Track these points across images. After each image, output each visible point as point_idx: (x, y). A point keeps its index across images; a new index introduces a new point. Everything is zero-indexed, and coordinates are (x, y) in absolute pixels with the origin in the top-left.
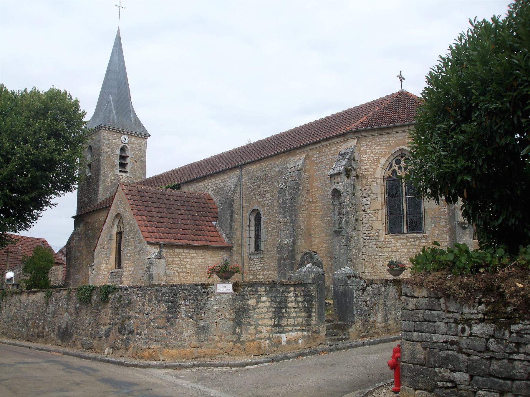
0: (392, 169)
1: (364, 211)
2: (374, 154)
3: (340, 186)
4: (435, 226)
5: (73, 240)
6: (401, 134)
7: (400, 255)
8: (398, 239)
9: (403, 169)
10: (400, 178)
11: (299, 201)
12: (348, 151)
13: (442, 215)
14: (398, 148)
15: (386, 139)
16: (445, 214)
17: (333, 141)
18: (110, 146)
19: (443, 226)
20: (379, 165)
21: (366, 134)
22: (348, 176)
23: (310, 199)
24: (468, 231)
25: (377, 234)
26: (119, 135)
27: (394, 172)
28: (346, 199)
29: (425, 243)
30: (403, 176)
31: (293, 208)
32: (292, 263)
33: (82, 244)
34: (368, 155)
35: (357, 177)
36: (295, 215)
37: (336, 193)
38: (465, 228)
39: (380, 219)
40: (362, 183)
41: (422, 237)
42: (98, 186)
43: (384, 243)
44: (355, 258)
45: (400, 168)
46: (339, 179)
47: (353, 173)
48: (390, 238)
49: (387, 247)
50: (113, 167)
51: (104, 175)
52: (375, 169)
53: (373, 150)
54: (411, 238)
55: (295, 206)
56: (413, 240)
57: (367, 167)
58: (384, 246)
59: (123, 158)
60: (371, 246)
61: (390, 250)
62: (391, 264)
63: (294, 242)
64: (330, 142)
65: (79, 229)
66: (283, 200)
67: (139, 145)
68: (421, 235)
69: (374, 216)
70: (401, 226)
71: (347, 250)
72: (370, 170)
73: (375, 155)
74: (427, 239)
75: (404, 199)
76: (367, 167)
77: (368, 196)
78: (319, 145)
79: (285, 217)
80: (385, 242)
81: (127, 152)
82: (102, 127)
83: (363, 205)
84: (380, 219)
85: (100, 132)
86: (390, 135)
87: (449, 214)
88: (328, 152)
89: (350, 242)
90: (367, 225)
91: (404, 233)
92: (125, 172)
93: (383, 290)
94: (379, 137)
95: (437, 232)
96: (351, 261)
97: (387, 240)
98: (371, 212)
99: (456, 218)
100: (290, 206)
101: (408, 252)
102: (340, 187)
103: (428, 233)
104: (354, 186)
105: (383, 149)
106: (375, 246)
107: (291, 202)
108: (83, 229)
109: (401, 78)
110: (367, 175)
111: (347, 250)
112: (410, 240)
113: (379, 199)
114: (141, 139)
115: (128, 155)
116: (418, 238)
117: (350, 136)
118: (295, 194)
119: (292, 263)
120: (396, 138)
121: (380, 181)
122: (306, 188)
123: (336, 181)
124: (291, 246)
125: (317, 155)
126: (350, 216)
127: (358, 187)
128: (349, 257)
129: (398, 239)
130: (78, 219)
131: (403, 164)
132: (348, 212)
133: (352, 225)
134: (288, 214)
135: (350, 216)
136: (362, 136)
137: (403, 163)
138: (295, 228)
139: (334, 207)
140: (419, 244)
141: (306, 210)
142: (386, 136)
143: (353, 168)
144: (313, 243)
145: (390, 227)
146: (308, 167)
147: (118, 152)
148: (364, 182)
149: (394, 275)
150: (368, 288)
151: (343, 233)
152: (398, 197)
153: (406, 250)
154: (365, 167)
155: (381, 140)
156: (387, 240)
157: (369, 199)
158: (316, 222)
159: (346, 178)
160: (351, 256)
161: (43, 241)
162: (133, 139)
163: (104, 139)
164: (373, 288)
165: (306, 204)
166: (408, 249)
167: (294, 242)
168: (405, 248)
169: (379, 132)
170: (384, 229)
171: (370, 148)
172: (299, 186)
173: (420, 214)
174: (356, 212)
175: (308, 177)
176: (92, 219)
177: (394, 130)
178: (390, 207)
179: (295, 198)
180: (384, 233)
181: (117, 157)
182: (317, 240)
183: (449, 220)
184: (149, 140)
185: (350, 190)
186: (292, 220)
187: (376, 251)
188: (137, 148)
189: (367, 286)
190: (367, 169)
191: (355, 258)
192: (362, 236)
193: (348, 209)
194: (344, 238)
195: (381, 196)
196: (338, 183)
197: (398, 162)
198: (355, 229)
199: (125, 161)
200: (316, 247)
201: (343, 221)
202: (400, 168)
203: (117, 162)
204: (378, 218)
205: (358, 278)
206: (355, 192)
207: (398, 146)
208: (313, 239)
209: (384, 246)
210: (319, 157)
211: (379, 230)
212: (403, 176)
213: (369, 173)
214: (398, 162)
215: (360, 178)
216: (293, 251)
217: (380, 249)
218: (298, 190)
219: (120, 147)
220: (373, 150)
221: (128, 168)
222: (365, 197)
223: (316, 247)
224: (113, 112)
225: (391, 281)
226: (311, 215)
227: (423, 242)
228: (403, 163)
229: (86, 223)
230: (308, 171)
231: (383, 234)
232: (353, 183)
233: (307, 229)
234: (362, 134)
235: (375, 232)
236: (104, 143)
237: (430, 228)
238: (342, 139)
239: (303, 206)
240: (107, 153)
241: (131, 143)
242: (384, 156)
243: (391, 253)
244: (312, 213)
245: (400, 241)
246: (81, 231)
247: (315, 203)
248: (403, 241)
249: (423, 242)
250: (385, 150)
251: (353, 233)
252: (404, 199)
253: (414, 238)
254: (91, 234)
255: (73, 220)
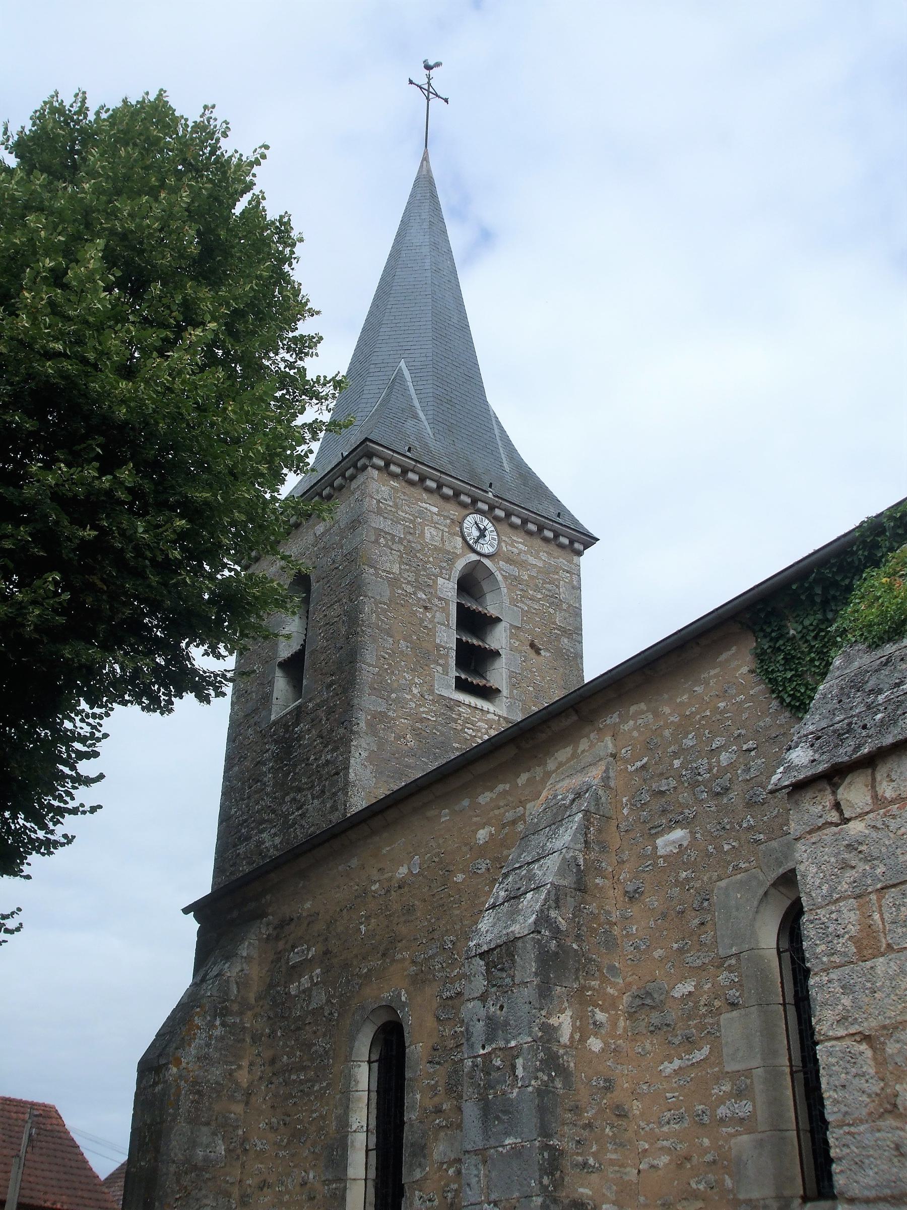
5: (184, 1043)
18: (410, 551)
26: (454, 511)
33: (243, 1077)
42: (343, 745)
50: (425, 656)
51: (381, 689)
59: (474, 622)
65: (232, 971)
67: (548, 571)
81: (489, 598)
82: (370, 455)
85: (361, 478)
92: (488, 693)
108: (256, 972)
114: (552, 547)
115: (492, 610)
130: (220, 918)
147: (448, 588)
161: (53, 1107)
162: (519, 544)
163: (379, 512)
176: (323, 897)
181: (445, 610)
184: (589, 559)
188: (537, 589)
199: (483, 641)
203: (448, 637)
219: (460, 564)
221: (498, 675)
224: (416, 417)
229: (283, 924)
236: (379, 532)
240: (394, 582)
241: (509, 561)
246: (243, 984)
254: (319, 998)
255: (192, 925)
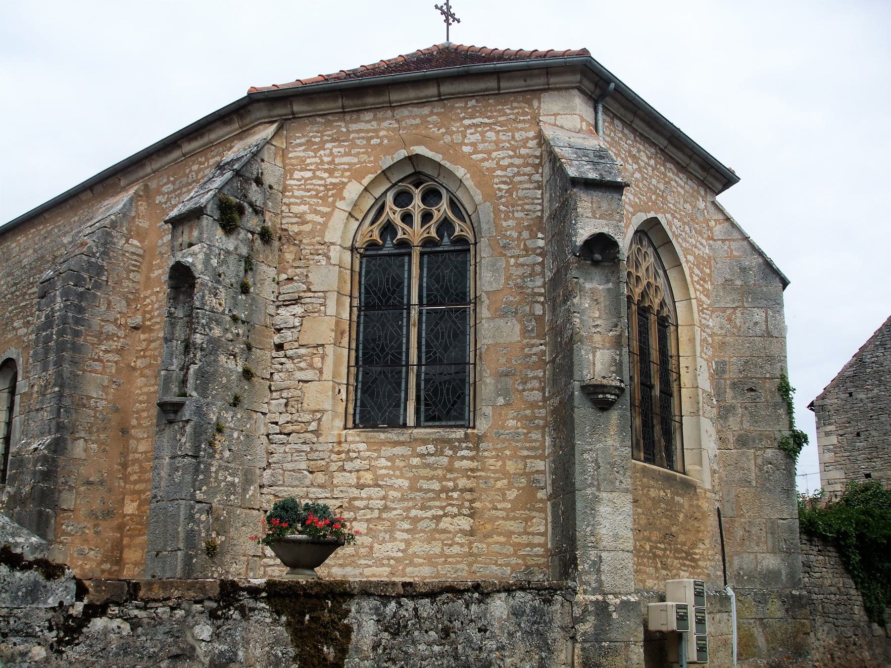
0: (383, 219)
1: (279, 347)
2: (326, 171)
3: (194, 254)
4: (507, 404)
6: (416, 111)
7: (384, 498)
8: (383, 443)
9: (417, 219)
10: (404, 244)
11: (96, 321)
12: (242, 154)
13: (533, 367)
14: (403, 154)
15: (368, 126)
16: (542, 364)
17: (213, 136)
19: (533, 405)
20: (338, 204)
21: (305, 108)
22: (229, 226)
23: (138, 320)
24: (614, 416)
25: (313, 426)
27: (389, 229)
28: (214, 300)
29: (472, 459)
30: (416, 241)
31: (68, 337)
32: (40, 514)
34: (309, 174)
35: (265, 236)
36: (74, 363)
37: (182, 279)
38: (604, 406)
39: (328, 374)
40: (281, 260)
41: (460, 441)
43: (334, 457)
44: (227, 505)
45: (407, 218)
46: (195, 233)
47: (251, 221)
48: (357, 440)
49: (342, 469)
52: (328, 216)
53: (326, 159)
54: (425, 442)
55: (77, 334)
56: (431, 448)
57: (305, 208)
58: (334, 467)
60: (289, 466)
61: (353, 481)
62: (285, 514)
63: (58, 447)
64: (205, 140)
66: (47, 317)
68: (460, 433)
69: (311, 366)
70: (398, 404)
71: (197, 471)
72: (309, 217)
73: (331, 172)
74: (476, 448)
75: (414, 313)
76: (305, 208)
77: (296, 301)
78: (176, 154)
79: (45, 369)
80: (339, 453)
83: (279, 330)
84: (328, 374)
86: (380, 115)
87: (553, 361)
88: (197, 173)
89: (211, 444)
90: (285, 394)
91: (405, 426)
93: (204, 631)
94: (348, 118)
95: (511, 423)
96: (209, 511)
97: (345, 447)
98: (303, 351)
99: (576, 368)
100: (61, 333)
101: (412, 488)
102: (194, 258)
103: (482, 426)
104: (249, 264)
105: (355, 155)
106: (303, 465)
107: (64, 320)
109: (448, 15)
110: (299, 233)
111: (197, 471)
112: (421, 449)
113: (331, 309)
116: (449, 442)
117: (258, 114)
118: (81, 296)
119: (40, 514)
120: (398, 121)
121: (341, 256)
122: (126, 283)
123: (185, 238)
124: (45, 460)
125: (170, 187)
126: (222, 358)
127: (264, 267)
128: (199, 495)
129: (383, 443)
131: (417, 206)
132: (213, 341)
133: (226, 387)
134: (52, 357)
135: (222, 358)
136: (294, 117)
137: (417, 201)
138: (67, 402)
139: (173, 325)
140: (451, 463)
141: (120, 351)
142: (368, 116)
143: (251, 204)
144: (131, 457)
145: (363, 405)
146: (144, 224)
148: (289, 257)
149: (294, 565)
150: (98, 623)
151: (187, 413)
152: (395, 307)
153: (406, 483)
154: (295, 209)
155: (354, 127)
156: (345, 447)
157: (298, 309)
158: (145, 390)
159: (219, 232)
160: (213, 492)
164: (135, 623)
165: (121, 333)
166: (414, 480)
167: (58, 447)
168: (402, 476)
169: (347, 102)
170: (341, 409)
171: (315, 151)
172: (99, 274)
173: (462, 364)
174: (249, 348)
175: (141, 252)
177: (395, 96)
178: (365, 339)
179: (81, 310)
180: (340, 423)
182: (141, 448)
183: (554, 381)
185: (233, 272)
186: (59, 374)
187: (307, 482)
189: (95, 611)
190: (300, 216)
191: (227, 505)
192: (263, 430)
193: (217, 332)
194: (188, 428)
195: (339, 303)
196: (191, 245)
197: (403, 199)
198: (236, 402)
200: (136, 468)
201: (193, 368)
202: (407, 218)
204: (321, 372)
205: (29, 566)
206: (250, 281)
207: (405, 146)
208: (132, 443)
209: (334, 467)
210: (174, 190)
211: (323, 411)
212: (416, 241)
213: (307, 228)
214: (403, 199)
215: (276, 244)
216: (47, 476)
217: (320, 478)
218: (97, 286)
220: (326, 159)
222: (287, 304)
223: (136, 468)
225: (254, 592)
226: (134, 369)
227: (463, 458)
228: (417, 201)
230: (141, 235)
231: (334, 426)
232: (244, 251)
233: (117, 410)
234: (296, 108)
235: (307, 417)
237: (488, 410)
238: (235, 127)
239: (110, 337)
242: (357, 176)
243: (355, 492)
244: (140, 363)
245: (388, 451)
247: (149, 329)
248: (399, 450)
249: (463, 458)
250: (364, 157)
251: (228, 416)
252: (414, 313)
253: (435, 441)
